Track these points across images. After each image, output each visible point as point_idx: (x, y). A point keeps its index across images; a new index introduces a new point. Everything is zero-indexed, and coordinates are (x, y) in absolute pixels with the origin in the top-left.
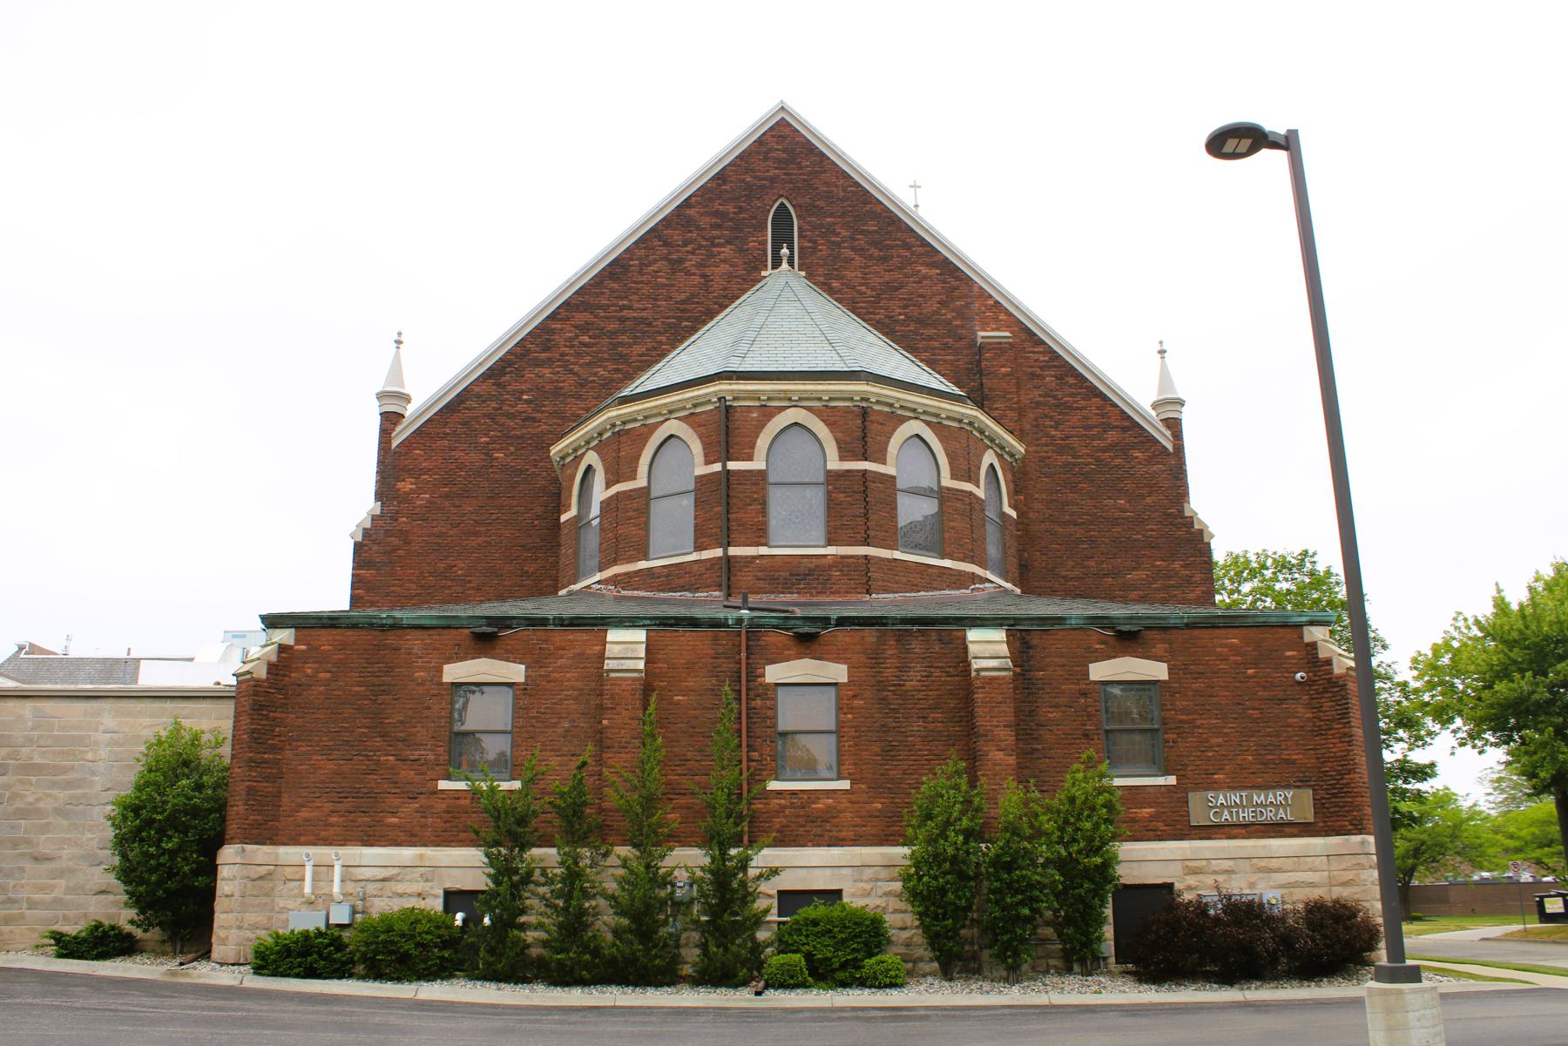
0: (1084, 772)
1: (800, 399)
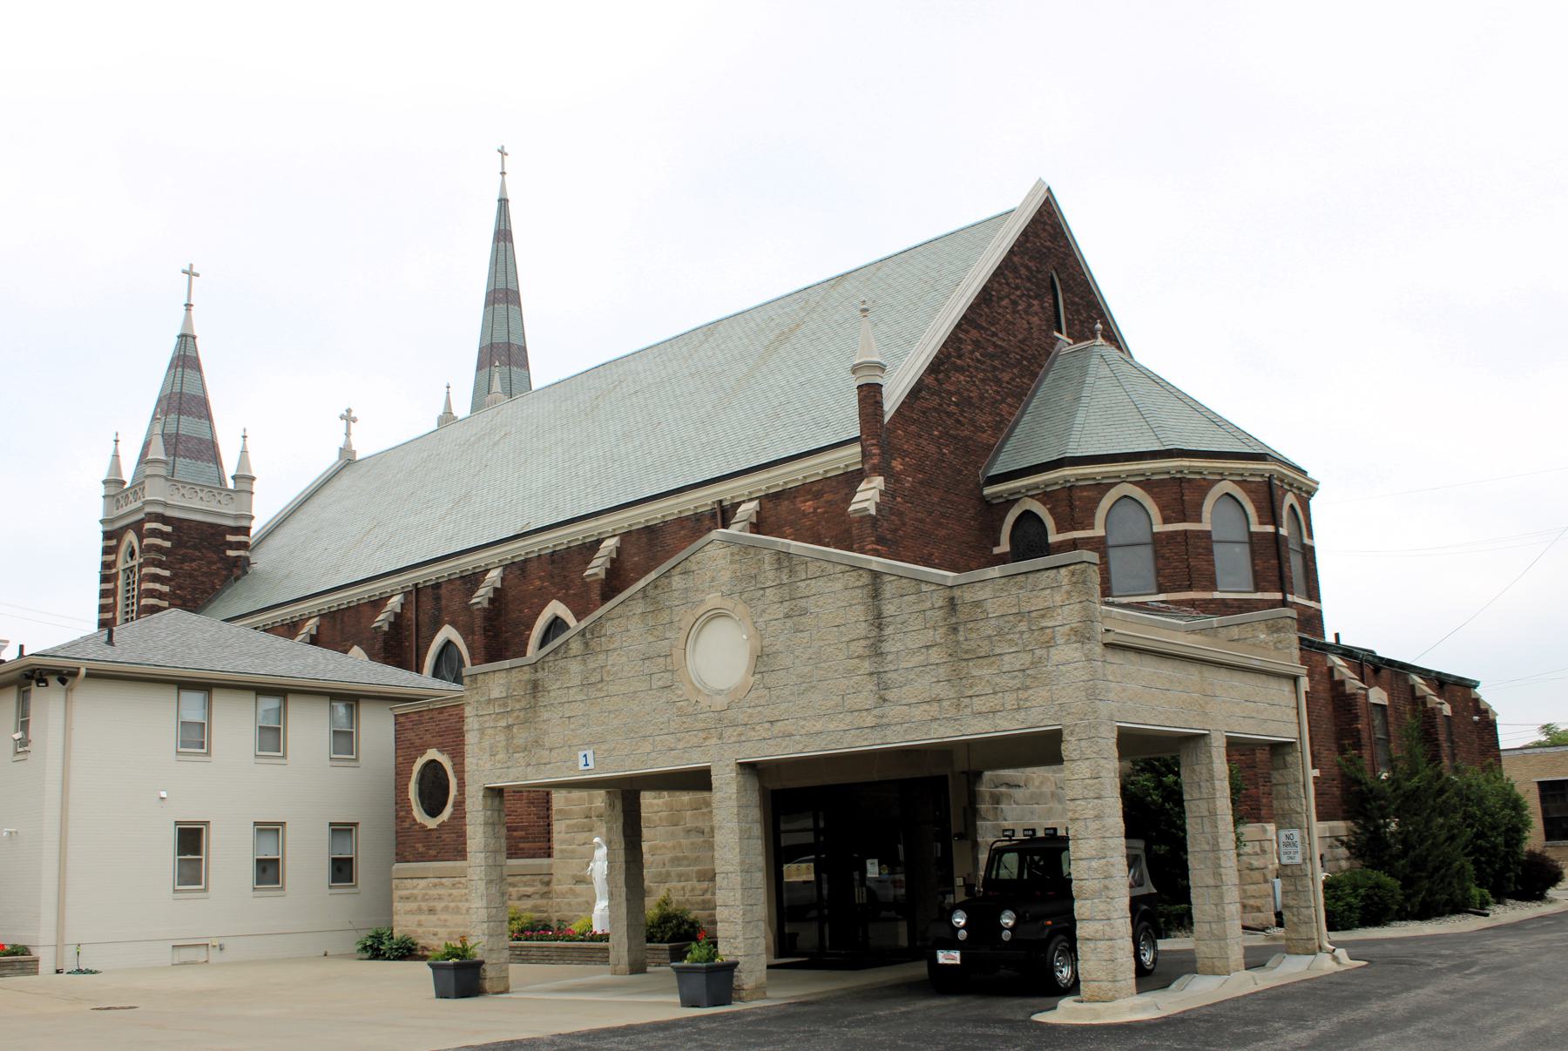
1: (1128, 476)
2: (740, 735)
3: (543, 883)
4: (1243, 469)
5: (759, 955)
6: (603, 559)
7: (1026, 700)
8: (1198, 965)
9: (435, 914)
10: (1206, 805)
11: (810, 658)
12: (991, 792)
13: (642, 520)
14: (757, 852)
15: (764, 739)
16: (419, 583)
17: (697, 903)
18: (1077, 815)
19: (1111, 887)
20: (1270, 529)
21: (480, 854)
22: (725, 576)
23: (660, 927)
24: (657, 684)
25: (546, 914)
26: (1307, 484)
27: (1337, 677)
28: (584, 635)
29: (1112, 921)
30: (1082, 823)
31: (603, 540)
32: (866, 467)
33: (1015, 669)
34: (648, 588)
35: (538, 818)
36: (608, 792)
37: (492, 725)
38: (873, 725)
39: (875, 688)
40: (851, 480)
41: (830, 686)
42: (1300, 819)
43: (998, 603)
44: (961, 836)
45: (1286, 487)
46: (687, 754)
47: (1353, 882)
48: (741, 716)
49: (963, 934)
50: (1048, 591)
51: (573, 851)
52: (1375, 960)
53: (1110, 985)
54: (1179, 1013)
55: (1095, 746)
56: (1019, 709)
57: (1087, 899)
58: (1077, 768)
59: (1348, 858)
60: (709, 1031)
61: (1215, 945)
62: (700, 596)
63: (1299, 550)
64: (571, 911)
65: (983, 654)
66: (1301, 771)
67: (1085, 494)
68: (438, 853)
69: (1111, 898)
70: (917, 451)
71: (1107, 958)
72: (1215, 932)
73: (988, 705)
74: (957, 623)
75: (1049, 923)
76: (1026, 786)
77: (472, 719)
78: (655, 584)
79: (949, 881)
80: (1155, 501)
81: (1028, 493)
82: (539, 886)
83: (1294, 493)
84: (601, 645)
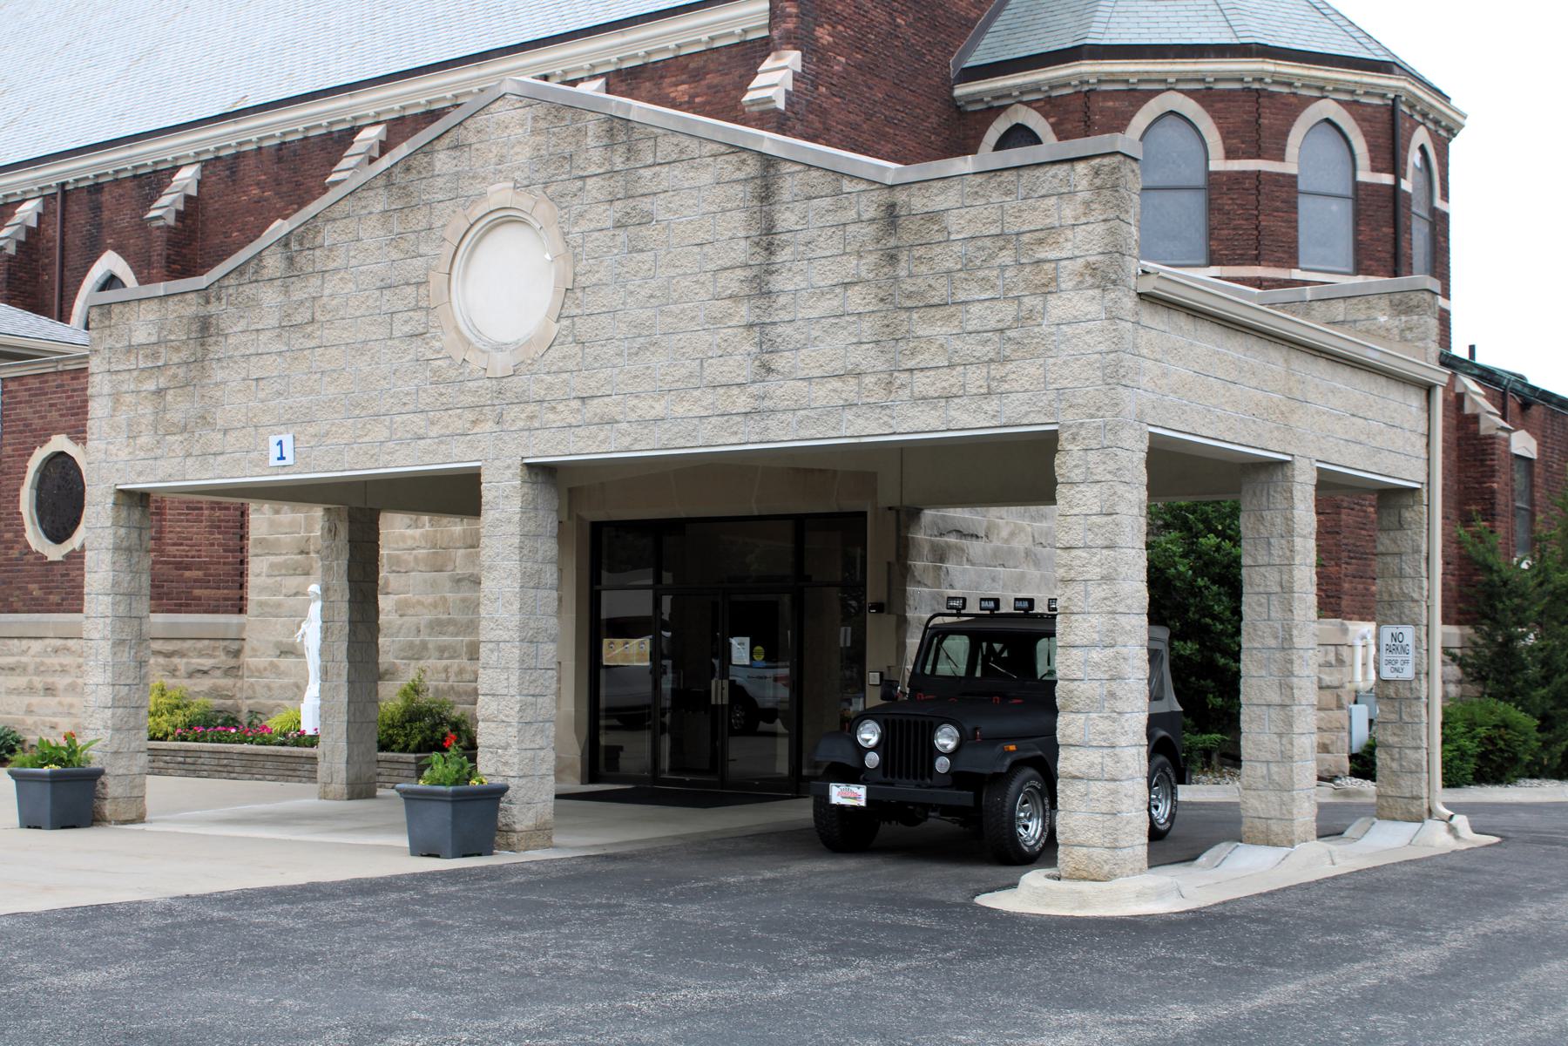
0: (1507, 627)
2: (531, 418)
3: (228, 652)
4: (1356, 82)
5: (543, 776)
6: (358, 158)
7: (1003, 379)
8: (1244, 828)
9: (54, 695)
10: (1277, 576)
11: (652, 296)
12: (931, 541)
13: (423, 101)
14: (549, 610)
15: (570, 426)
16: (67, 183)
17: (466, 693)
18: (1072, 574)
19: (1120, 693)
20: (1387, 179)
21: (106, 598)
22: (522, 155)
23: (404, 727)
24: (401, 329)
25: (230, 702)
26: (1448, 117)
27: (1468, 409)
28: (287, 245)
29: (1117, 750)
30: (1080, 587)
31: (360, 128)
32: (776, 33)
33: (988, 328)
34: (396, 170)
35: (225, 551)
36: (327, 510)
37: (132, 387)
38: (748, 410)
39: (755, 350)
40: (750, 54)
41: (681, 344)
42: (1416, 609)
43: (968, 217)
44: (879, 608)
45: (1417, 117)
46: (443, 447)
47: (1468, 716)
48: (534, 388)
49: (872, 759)
50: (1053, 200)
51: (279, 605)
52: (1510, 834)
53: (1107, 854)
54: (1216, 905)
55: (1111, 463)
56: (989, 394)
57: (1078, 712)
58: (1079, 496)
59: (1460, 682)
60: (443, 899)
61: (1273, 799)
62: (479, 186)
63: (1425, 215)
64: (270, 697)
65: (936, 300)
66: (1425, 535)
67: (1110, 104)
68: (63, 600)
69: (1119, 713)
70: (856, 17)
71: (1104, 809)
72: (1276, 777)
73: (939, 385)
74: (897, 247)
75: (1012, 748)
76: (987, 536)
77: (100, 376)
78: (406, 165)
79: (860, 685)
80: (1216, 123)
81: (1022, 97)
82: (223, 657)
83: (1428, 129)
84: (314, 261)
